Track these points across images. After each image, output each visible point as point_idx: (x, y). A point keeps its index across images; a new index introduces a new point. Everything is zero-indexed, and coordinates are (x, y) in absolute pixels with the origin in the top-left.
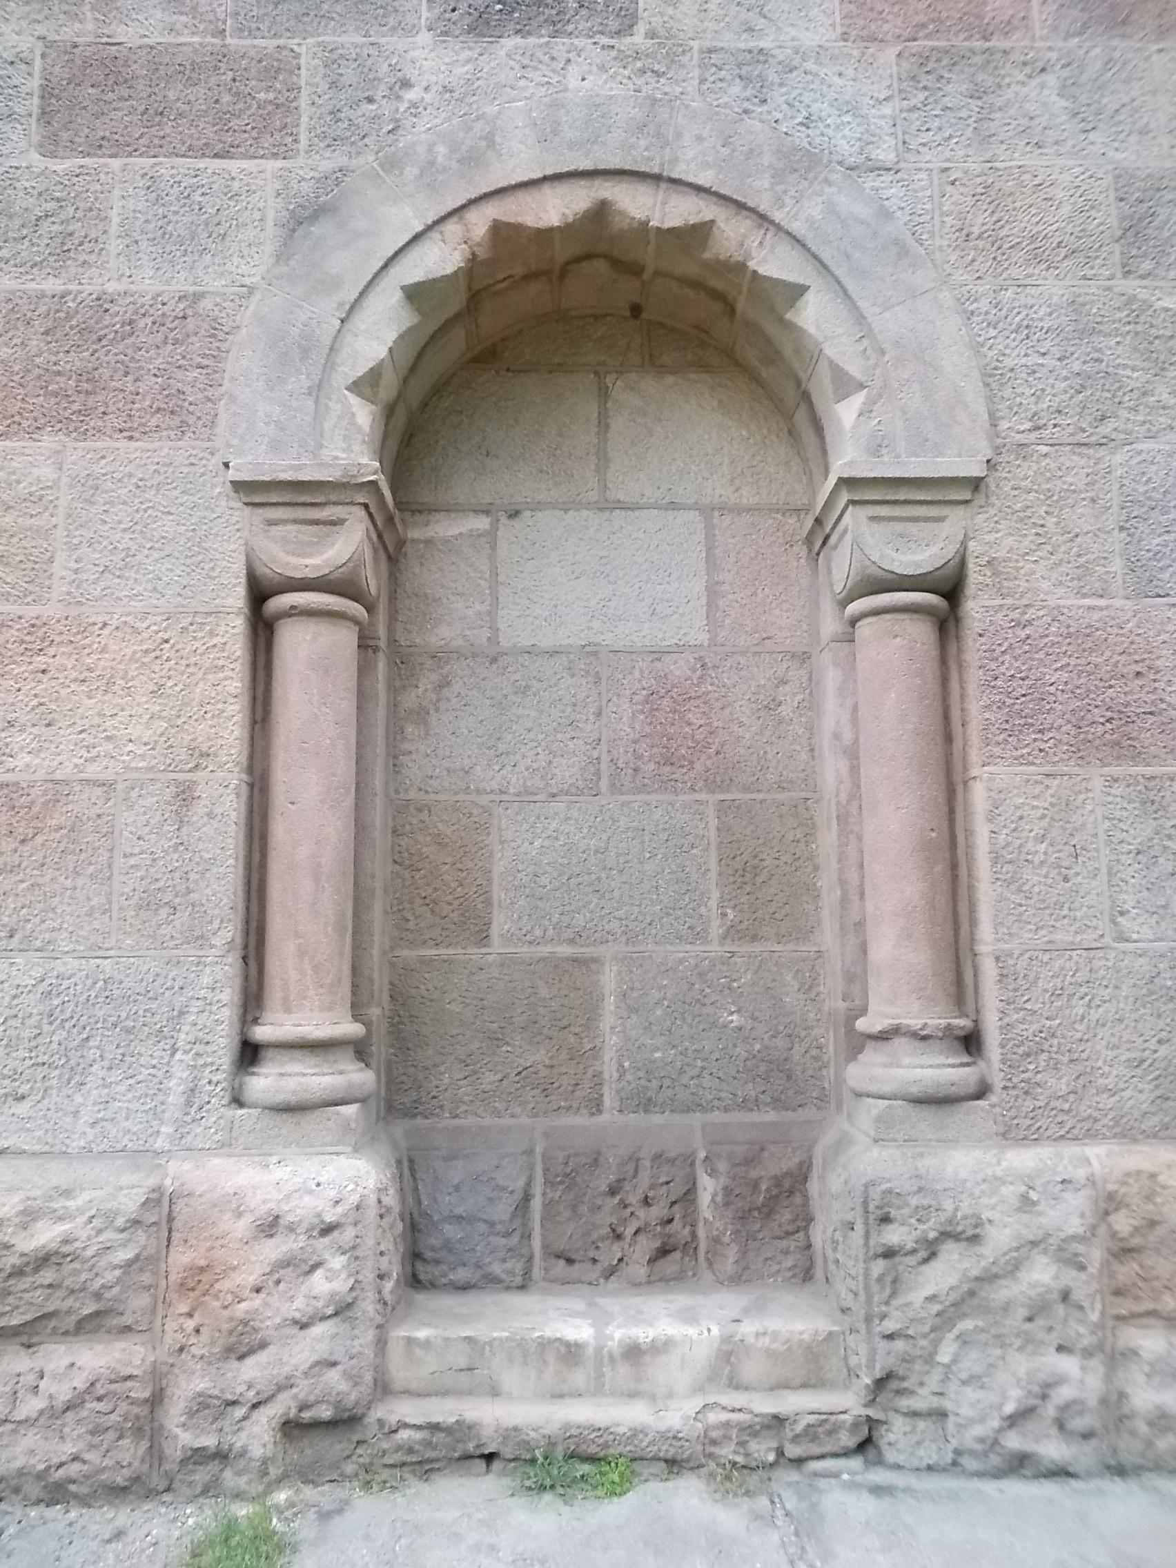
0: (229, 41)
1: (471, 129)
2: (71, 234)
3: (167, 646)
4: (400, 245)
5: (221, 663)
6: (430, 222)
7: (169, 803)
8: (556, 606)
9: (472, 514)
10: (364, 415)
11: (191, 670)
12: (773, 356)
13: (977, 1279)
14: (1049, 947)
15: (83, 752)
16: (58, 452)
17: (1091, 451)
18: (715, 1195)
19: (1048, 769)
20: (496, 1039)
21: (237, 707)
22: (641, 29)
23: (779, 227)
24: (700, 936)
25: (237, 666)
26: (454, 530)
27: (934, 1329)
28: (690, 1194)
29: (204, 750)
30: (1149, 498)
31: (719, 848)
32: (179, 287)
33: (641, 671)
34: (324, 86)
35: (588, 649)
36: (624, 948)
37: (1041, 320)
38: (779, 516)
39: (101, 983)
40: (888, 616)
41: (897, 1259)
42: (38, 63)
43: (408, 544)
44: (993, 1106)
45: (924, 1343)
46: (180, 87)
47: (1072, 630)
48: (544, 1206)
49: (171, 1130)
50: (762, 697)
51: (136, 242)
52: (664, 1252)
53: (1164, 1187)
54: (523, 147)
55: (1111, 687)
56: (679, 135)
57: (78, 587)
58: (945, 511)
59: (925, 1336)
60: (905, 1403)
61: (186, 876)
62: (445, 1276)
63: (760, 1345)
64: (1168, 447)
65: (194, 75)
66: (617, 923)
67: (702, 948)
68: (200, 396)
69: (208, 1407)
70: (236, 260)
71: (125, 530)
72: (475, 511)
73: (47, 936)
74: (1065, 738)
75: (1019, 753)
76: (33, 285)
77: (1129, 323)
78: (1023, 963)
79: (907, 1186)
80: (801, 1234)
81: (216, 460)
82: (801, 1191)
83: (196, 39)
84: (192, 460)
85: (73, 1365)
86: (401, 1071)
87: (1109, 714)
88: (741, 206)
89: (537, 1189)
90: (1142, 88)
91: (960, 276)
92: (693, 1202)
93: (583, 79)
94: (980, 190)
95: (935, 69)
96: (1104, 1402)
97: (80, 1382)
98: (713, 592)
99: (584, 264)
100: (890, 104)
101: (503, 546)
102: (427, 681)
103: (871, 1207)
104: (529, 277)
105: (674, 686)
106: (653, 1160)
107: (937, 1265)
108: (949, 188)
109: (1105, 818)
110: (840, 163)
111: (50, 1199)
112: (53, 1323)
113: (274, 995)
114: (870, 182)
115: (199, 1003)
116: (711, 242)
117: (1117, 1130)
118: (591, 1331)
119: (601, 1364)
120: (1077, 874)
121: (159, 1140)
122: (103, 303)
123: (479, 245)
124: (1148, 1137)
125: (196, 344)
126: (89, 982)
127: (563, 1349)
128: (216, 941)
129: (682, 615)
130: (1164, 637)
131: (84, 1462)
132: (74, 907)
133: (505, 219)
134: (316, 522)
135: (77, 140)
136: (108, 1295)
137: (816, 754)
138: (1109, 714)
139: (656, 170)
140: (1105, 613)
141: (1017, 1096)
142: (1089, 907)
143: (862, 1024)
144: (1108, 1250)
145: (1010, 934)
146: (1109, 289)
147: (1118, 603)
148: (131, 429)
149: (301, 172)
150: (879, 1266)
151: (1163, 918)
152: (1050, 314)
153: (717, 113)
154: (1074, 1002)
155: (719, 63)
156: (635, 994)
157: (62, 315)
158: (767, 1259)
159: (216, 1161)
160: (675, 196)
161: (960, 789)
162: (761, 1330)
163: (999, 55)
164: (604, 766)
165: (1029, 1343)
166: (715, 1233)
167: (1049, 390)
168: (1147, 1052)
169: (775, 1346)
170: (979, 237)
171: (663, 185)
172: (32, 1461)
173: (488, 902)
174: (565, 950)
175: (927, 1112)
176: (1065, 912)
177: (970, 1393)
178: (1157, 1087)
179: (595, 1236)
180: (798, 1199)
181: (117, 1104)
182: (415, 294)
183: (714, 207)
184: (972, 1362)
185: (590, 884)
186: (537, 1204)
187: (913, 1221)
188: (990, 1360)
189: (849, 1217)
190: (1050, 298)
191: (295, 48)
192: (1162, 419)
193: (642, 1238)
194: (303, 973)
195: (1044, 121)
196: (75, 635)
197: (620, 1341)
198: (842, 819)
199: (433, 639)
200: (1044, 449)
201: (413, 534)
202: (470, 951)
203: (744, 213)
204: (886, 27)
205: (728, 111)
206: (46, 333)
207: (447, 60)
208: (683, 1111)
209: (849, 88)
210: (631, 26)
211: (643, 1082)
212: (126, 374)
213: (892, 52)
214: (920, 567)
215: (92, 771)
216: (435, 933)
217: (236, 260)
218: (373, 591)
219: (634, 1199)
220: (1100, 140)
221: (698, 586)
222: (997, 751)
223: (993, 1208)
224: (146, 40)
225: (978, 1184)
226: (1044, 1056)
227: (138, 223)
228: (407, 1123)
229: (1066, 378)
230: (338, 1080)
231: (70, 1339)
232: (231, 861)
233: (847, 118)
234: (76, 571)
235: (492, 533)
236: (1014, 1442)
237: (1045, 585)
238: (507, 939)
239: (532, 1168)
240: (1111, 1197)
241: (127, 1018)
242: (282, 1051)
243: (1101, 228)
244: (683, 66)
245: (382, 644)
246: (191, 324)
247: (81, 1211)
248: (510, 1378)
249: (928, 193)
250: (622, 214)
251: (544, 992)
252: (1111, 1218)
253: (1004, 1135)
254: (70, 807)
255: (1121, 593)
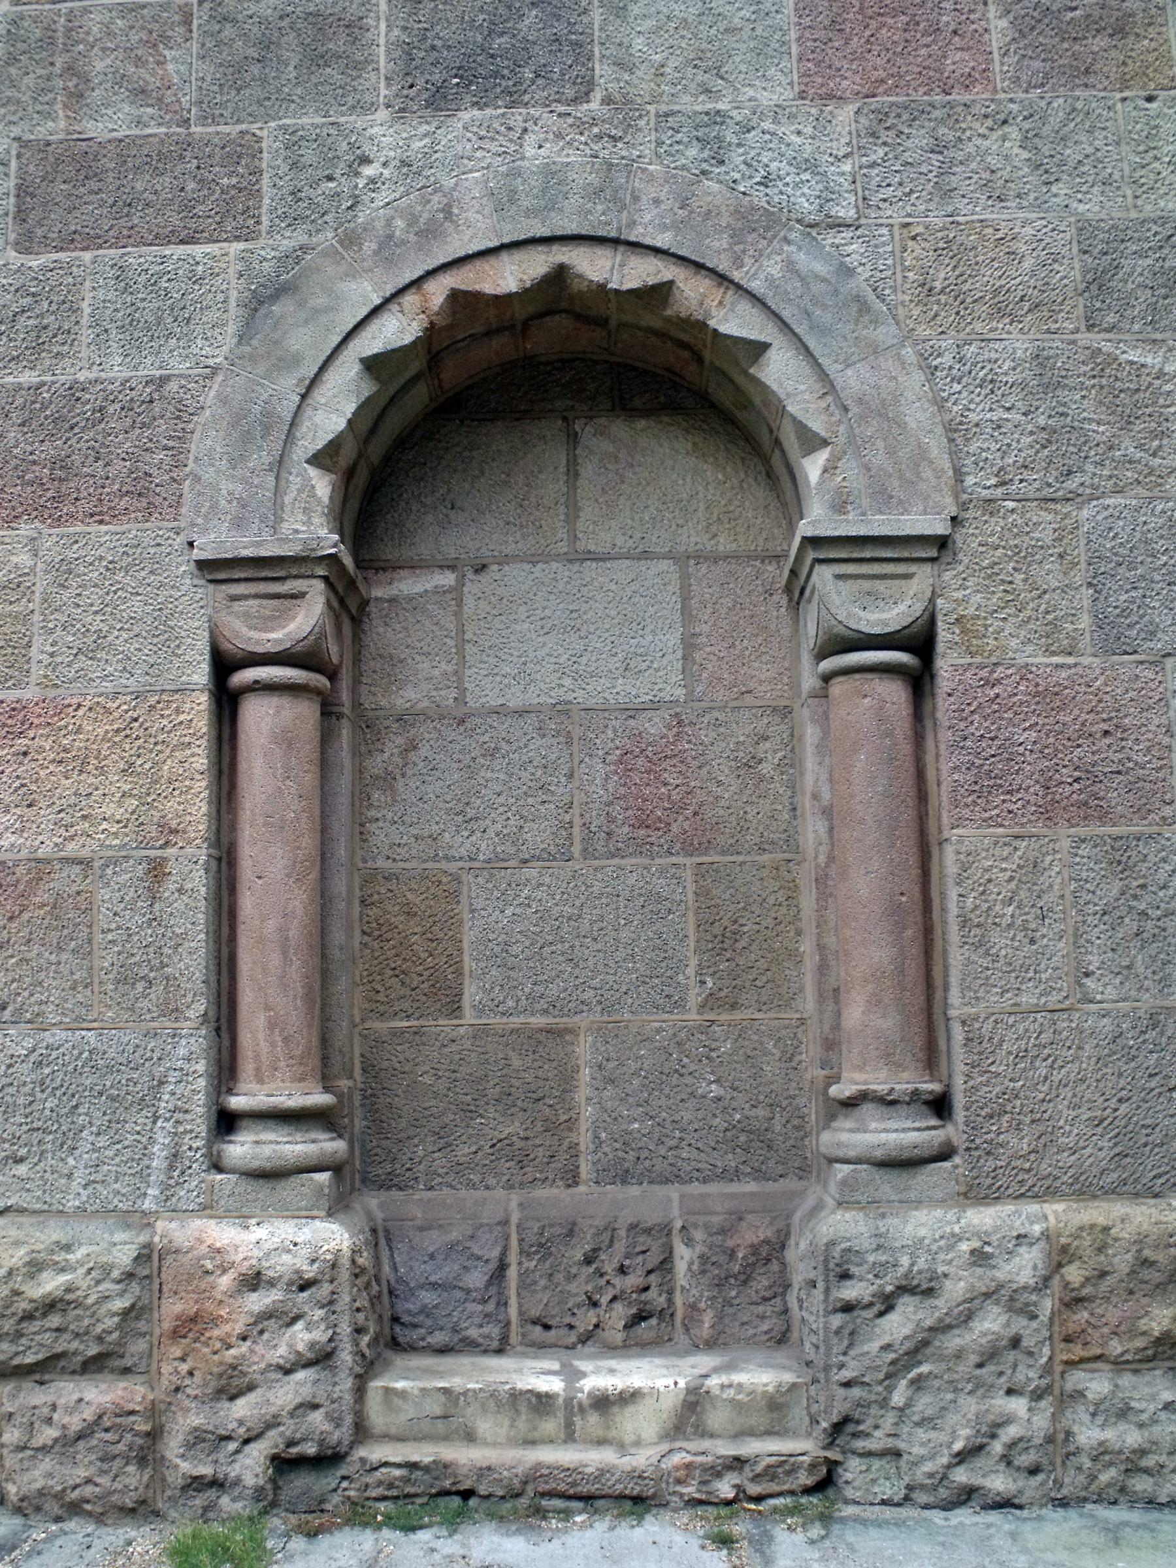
0: (193, 129)
1: (429, 201)
2: (45, 328)
3: (136, 724)
4: (359, 318)
5: (187, 739)
6: (388, 294)
7: (142, 880)
8: (525, 664)
9: (437, 570)
10: (322, 485)
11: (159, 747)
12: (746, 403)
13: (931, 1329)
14: (1016, 1009)
15: (62, 831)
16: (34, 539)
17: (1059, 506)
18: (691, 1263)
19: (1017, 830)
20: (469, 1112)
21: (204, 784)
22: (598, 95)
23: (739, 287)
24: (680, 1005)
25: (203, 742)
26: (418, 588)
27: (888, 1376)
28: (666, 1264)
29: (173, 826)
30: (1116, 554)
31: (697, 914)
32: (146, 372)
33: (615, 731)
34: (285, 168)
35: (559, 707)
36: (598, 1017)
37: (1006, 374)
38: (758, 563)
39: (86, 1054)
40: (857, 676)
41: (856, 1313)
42: (14, 164)
43: (372, 604)
44: (956, 1167)
45: (880, 1389)
46: (148, 177)
47: (1040, 689)
48: (520, 1275)
49: (157, 1192)
50: (741, 754)
51: (106, 331)
52: (640, 1317)
53: (1116, 1240)
54: (479, 217)
55: (1079, 746)
56: (636, 199)
57: (54, 670)
58: (913, 568)
59: (880, 1383)
60: (859, 1444)
61: (159, 952)
62: (423, 1339)
63: (724, 1396)
64: (1134, 502)
65: (160, 165)
66: (591, 993)
67: (679, 1017)
68: (166, 477)
69: (204, 1440)
70: (199, 342)
71: (96, 613)
72: (441, 567)
73: (36, 1008)
74: (1033, 799)
75: (987, 815)
76: (10, 379)
77: (1094, 377)
78: (988, 1026)
79: (866, 1244)
80: (778, 1300)
81: (180, 540)
82: (778, 1259)
83: (163, 130)
84: (159, 540)
85: (81, 1400)
86: (375, 1143)
87: (1077, 774)
88: (699, 266)
89: (513, 1258)
90: (1106, 138)
91: (923, 331)
92: (670, 1271)
93: (540, 147)
94: (941, 245)
95: (894, 126)
96: (1050, 1440)
97: (89, 1414)
98: (689, 645)
99: (548, 319)
100: (850, 161)
101: (469, 602)
102: (393, 746)
103: (832, 1266)
104: (488, 334)
105: (650, 744)
106: (628, 1230)
107: (893, 1318)
108: (910, 243)
109: (1071, 879)
110: (798, 221)
111: (52, 1252)
112: (62, 1363)
113: (247, 1067)
114: (830, 239)
115: (176, 1074)
116: (671, 300)
117: (1078, 1186)
118: (562, 1384)
119: (572, 1414)
120: (1044, 936)
121: (147, 1202)
122: (74, 391)
123: (438, 314)
124: (1106, 1193)
125: (162, 427)
126: (75, 1052)
127: (534, 1400)
128: (191, 1014)
129: (657, 670)
130: (1131, 694)
131: (96, 1485)
132: (58, 982)
133: (463, 287)
134: (277, 596)
135: (51, 235)
136: (109, 1339)
137: (798, 813)
138: (1077, 774)
139: (613, 234)
140: (1073, 671)
141: (980, 1157)
142: (1055, 969)
143: (834, 1091)
144: (1061, 1300)
145: (977, 998)
146: (1074, 342)
147: (1086, 661)
148: (101, 513)
149: (263, 253)
150: (837, 1320)
151: (1127, 978)
152: (1014, 369)
153: (674, 176)
154: (1037, 1064)
155: (675, 126)
156: (611, 1065)
157: (38, 406)
158: (743, 1324)
159: (198, 1222)
160: (633, 258)
161: (935, 851)
162: (726, 1382)
163: (959, 109)
164: (576, 830)
165: (980, 1387)
166: (692, 1300)
167: (1014, 444)
168: (1109, 1111)
169: (740, 1397)
170: (942, 291)
171: (621, 248)
172: (50, 1483)
173: (459, 972)
174: (538, 1021)
175: (892, 1175)
176: (1031, 974)
177: (921, 1434)
178: (1116, 1144)
179: (570, 1305)
180: (775, 1266)
181: (106, 1167)
182: (373, 365)
183: (672, 268)
184: (925, 1403)
185: (563, 954)
186: (512, 1273)
187: (870, 1276)
188: (942, 1404)
189: (812, 1275)
190: (1014, 352)
191: (258, 132)
192: (1129, 474)
193: (618, 1307)
194: (273, 1045)
195: (1005, 174)
196: (52, 716)
197: (589, 1393)
198: (821, 880)
199: (399, 702)
200: (1011, 505)
201: (377, 592)
202: (441, 1022)
203: (703, 272)
204: (845, 83)
205: (685, 173)
206: (23, 424)
207: (404, 135)
208: (661, 1183)
209: (807, 147)
210: (587, 94)
211: (620, 1154)
212: (97, 460)
213: (852, 108)
214: (887, 625)
215: (71, 849)
216: (405, 1005)
217: (199, 342)
218: (335, 660)
219: (609, 1268)
220: (1062, 192)
221: (673, 640)
222: (966, 812)
223: (950, 1262)
224: (115, 134)
225: (935, 1241)
226: (1007, 1117)
227: (108, 312)
228: (384, 1195)
229: (1032, 433)
230: (311, 1148)
231: (77, 1377)
232: (202, 936)
233: (806, 176)
234: (52, 655)
235: (457, 591)
236: (961, 1476)
237: (1014, 642)
238: (480, 1010)
239: (507, 1238)
240: (1064, 1249)
241: (112, 1087)
242: (258, 1121)
243: (1065, 281)
244: (640, 130)
245: (346, 710)
246: (157, 408)
247: (81, 1263)
248: (484, 1426)
249: (889, 248)
250: (580, 276)
251: (516, 1063)
252: (1063, 1270)
253: (965, 1194)
254: (52, 885)
255: (1089, 650)
